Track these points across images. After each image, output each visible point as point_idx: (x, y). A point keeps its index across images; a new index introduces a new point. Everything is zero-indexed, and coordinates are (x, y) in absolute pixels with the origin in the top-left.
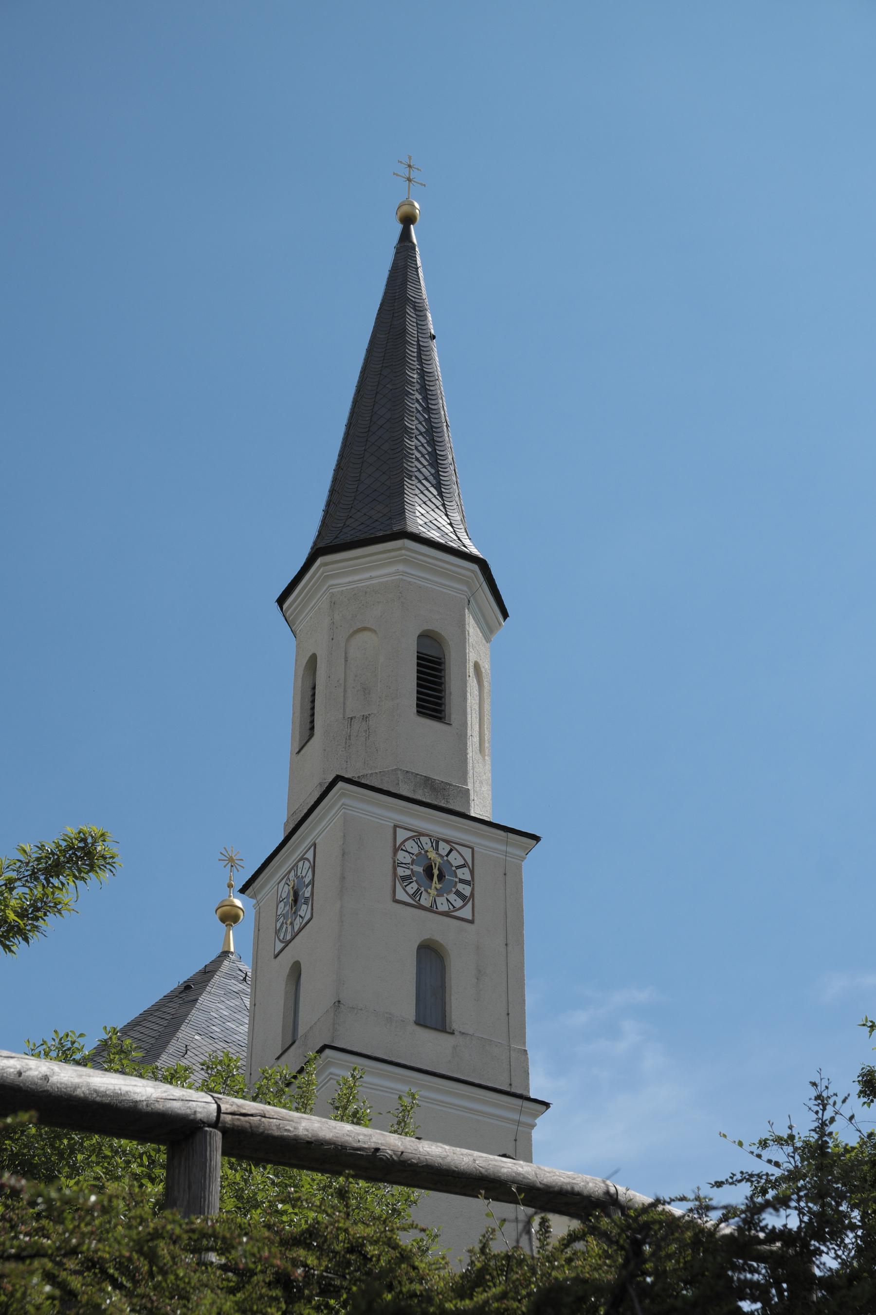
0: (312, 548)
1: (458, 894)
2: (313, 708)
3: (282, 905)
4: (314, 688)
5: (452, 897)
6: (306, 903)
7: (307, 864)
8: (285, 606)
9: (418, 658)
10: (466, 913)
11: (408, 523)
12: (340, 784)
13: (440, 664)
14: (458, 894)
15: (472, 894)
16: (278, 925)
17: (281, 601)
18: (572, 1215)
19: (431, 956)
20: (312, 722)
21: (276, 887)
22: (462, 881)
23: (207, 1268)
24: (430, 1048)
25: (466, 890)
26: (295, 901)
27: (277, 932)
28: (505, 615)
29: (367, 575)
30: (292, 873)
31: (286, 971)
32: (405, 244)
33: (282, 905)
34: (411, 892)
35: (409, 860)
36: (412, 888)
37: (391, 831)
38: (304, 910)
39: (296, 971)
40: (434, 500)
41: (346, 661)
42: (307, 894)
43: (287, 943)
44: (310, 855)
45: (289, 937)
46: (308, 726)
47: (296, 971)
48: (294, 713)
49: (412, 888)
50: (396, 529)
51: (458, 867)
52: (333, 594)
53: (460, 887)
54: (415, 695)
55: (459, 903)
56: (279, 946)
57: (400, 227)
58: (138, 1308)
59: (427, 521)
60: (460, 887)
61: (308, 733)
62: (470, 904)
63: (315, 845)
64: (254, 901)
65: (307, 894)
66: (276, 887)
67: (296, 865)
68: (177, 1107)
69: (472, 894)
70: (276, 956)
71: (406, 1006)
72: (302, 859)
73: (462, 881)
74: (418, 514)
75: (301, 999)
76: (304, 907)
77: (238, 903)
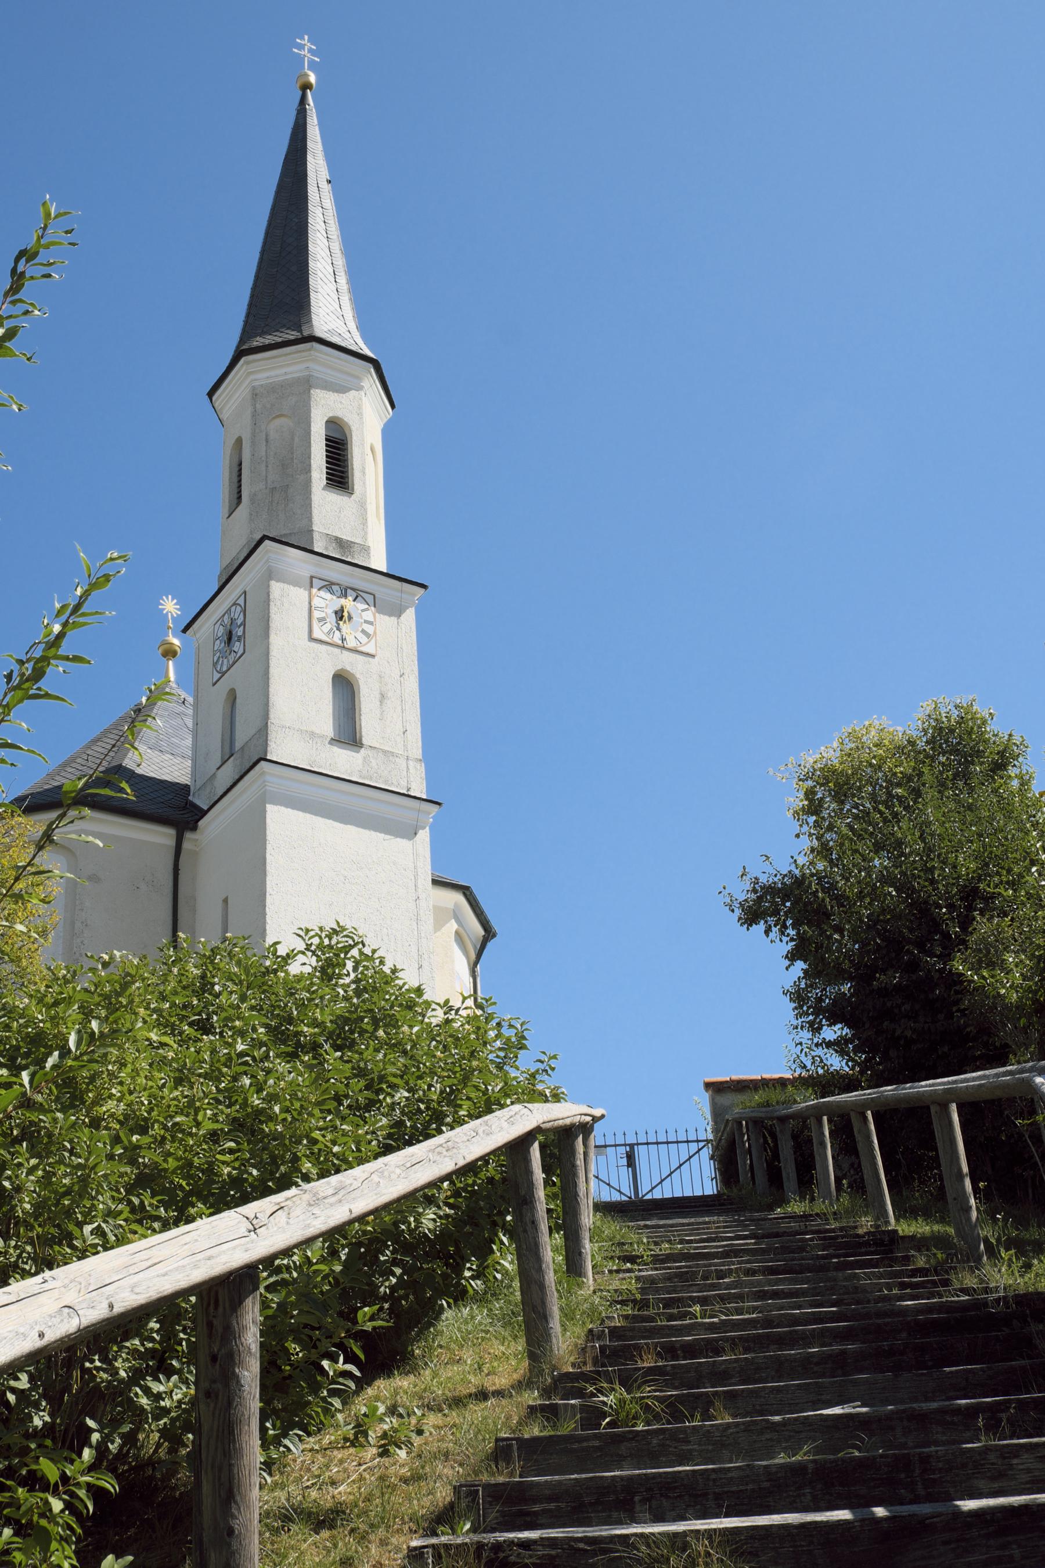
0: (235, 351)
1: (363, 631)
2: (240, 481)
3: (218, 642)
4: (240, 464)
5: (360, 636)
6: (239, 640)
7: (239, 609)
8: (214, 398)
9: (327, 440)
10: (369, 648)
11: (315, 329)
12: (267, 542)
13: (343, 444)
14: (363, 631)
15: (375, 632)
16: (216, 659)
17: (211, 394)
19: (344, 685)
20: (240, 492)
21: (209, 626)
22: (366, 622)
24: (343, 762)
25: (369, 629)
26: (230, 639)
27: (215, 664)
28: (436, 882)
29: (283, 371)
30: (226, 616)
31: (224, 695)
33: (218, 642)
35: (324, 605)
37: (308, 581)
38: (237, 646)
39: (232, 697)
40: (332, 303)
41: (267, 442)
42: (240, 633)
43: (223, 674)
44: (241, 601)
45: (225, 669)
46: (236, 496)
47: (232, 697)
49: (327, 628)
50: (306, 333)
51: (363, 611)
52: (254, 388)
53: (366, 627)
54: (325, 470)
55: (364, 639)
56: (217, 676)
57: (300, 93)
58: (476, 1073)
59: (328, 311)
60: (366, 627)
61: (236, 501)
62: (373, 641)
63: (245, 592)
65: (240, 633)
66: (209, 626)
68: (818, 1514)
69: (375, 632)
70: (214, 684)
71: (326, 725)
72: (235, 604)
73: (366, 622)
74: (321, 304)
75: (237, 724)
76: (237, 643)
77: (176, 642)
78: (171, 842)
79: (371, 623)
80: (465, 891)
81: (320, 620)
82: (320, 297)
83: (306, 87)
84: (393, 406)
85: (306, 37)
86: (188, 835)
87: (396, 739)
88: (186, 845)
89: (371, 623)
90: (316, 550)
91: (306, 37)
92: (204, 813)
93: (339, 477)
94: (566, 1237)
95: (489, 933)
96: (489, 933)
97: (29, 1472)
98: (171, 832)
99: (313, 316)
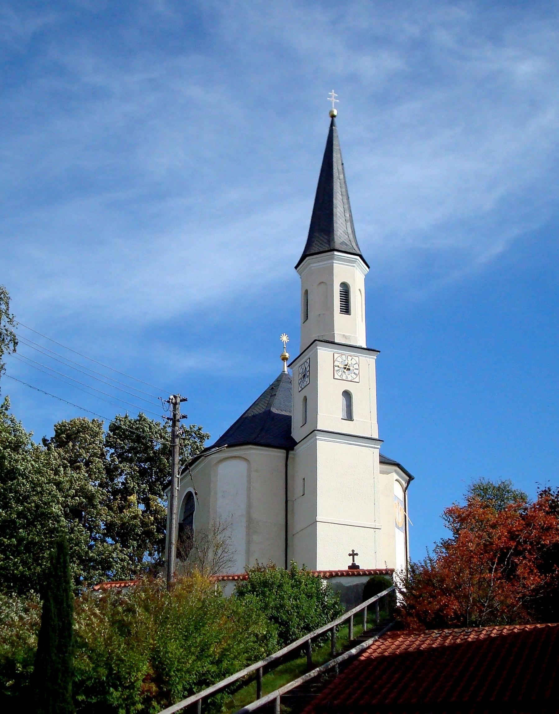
5: (353, 375)
17: (296, 267)
18: (39, 644)
19: (347, 395)
23: (42, 487)
25: (357, 372)
27: (299, 384)
32: (332, 124)
34: (340, 375)
36: (340, 374)
38: (307, 379)
39: (305, 399)
47: (305, 399)
48: (293, 510)
49: (340, 374)
53: (355, 371)
54: (339, 297)
55: (355, 376)
56: (300, 389)
57: (330, 119)
60: (355, 371)
64: (292, 370)
67: (304, 363)
78: (285, 455)
79: (357, 369)
80: (398, 465)
81: (337, 371)
82: (338, 225)
83: (333, 116)
84: (369, 267)
85: (333, 91)
86: (291, 452)
87: (366, 421)
88: (290, 456)
89: (357, 369)
90: (336, 341)
91: (333, 91)
92: (296, 444)
93: (346, 309)
94: (126, 711)
95: (411, 478)
96: (411, 478)
97: (547, 549)
98: (285, 451)
99: (335, 237)
